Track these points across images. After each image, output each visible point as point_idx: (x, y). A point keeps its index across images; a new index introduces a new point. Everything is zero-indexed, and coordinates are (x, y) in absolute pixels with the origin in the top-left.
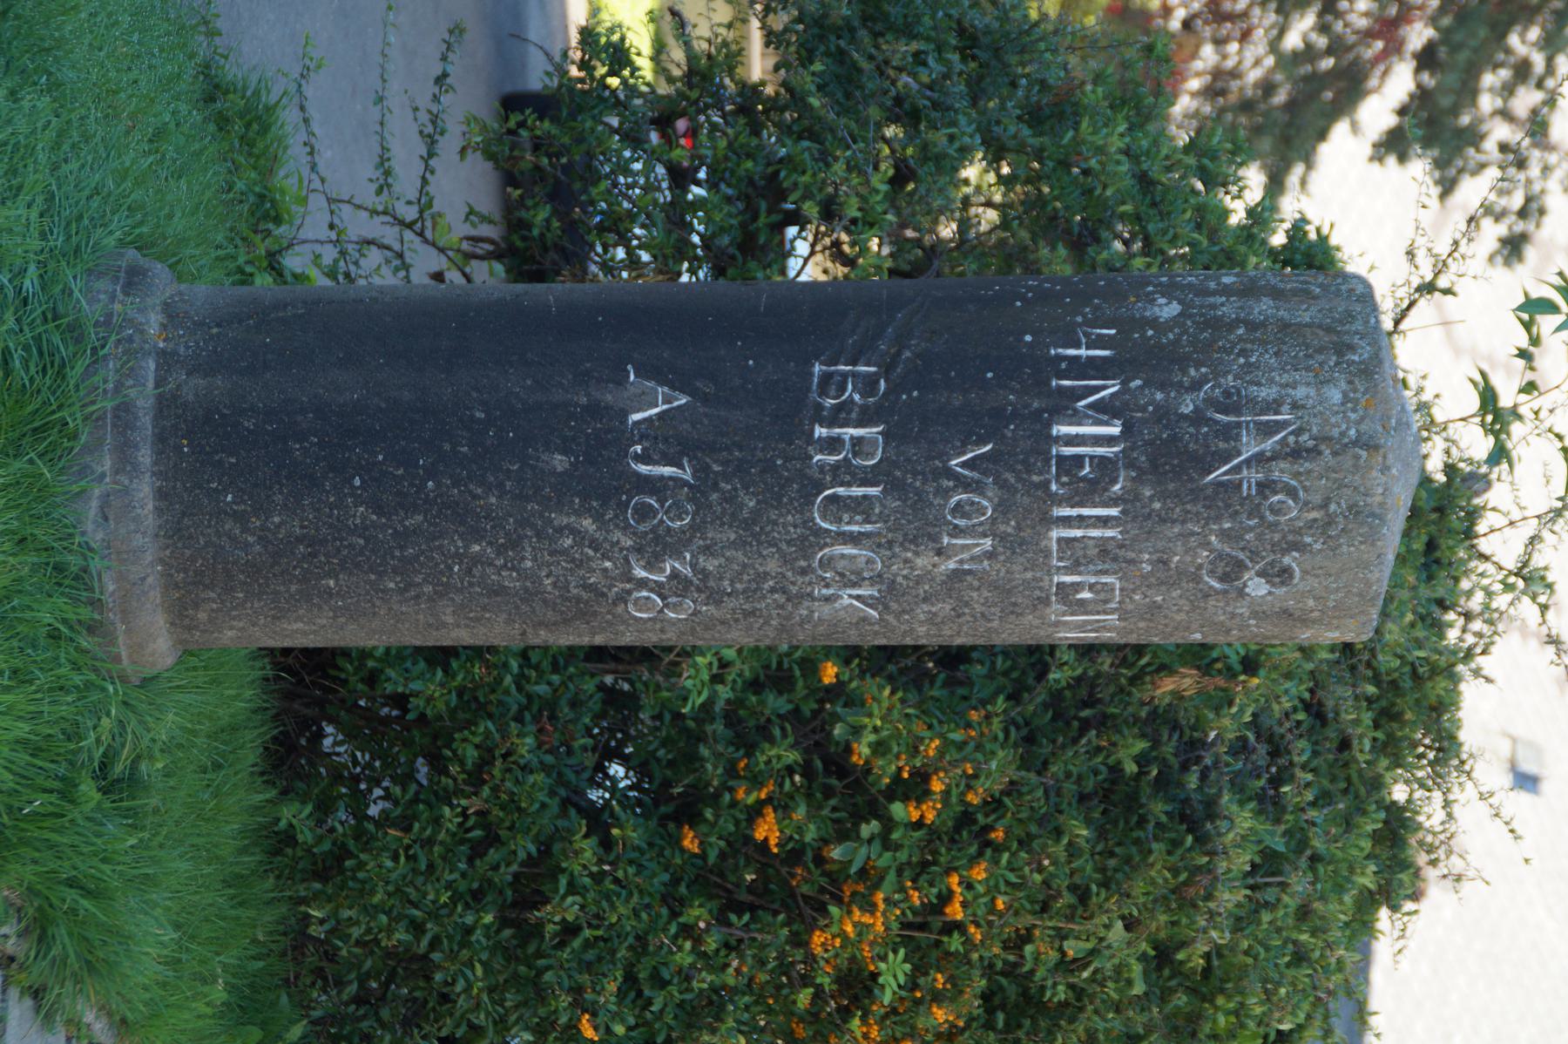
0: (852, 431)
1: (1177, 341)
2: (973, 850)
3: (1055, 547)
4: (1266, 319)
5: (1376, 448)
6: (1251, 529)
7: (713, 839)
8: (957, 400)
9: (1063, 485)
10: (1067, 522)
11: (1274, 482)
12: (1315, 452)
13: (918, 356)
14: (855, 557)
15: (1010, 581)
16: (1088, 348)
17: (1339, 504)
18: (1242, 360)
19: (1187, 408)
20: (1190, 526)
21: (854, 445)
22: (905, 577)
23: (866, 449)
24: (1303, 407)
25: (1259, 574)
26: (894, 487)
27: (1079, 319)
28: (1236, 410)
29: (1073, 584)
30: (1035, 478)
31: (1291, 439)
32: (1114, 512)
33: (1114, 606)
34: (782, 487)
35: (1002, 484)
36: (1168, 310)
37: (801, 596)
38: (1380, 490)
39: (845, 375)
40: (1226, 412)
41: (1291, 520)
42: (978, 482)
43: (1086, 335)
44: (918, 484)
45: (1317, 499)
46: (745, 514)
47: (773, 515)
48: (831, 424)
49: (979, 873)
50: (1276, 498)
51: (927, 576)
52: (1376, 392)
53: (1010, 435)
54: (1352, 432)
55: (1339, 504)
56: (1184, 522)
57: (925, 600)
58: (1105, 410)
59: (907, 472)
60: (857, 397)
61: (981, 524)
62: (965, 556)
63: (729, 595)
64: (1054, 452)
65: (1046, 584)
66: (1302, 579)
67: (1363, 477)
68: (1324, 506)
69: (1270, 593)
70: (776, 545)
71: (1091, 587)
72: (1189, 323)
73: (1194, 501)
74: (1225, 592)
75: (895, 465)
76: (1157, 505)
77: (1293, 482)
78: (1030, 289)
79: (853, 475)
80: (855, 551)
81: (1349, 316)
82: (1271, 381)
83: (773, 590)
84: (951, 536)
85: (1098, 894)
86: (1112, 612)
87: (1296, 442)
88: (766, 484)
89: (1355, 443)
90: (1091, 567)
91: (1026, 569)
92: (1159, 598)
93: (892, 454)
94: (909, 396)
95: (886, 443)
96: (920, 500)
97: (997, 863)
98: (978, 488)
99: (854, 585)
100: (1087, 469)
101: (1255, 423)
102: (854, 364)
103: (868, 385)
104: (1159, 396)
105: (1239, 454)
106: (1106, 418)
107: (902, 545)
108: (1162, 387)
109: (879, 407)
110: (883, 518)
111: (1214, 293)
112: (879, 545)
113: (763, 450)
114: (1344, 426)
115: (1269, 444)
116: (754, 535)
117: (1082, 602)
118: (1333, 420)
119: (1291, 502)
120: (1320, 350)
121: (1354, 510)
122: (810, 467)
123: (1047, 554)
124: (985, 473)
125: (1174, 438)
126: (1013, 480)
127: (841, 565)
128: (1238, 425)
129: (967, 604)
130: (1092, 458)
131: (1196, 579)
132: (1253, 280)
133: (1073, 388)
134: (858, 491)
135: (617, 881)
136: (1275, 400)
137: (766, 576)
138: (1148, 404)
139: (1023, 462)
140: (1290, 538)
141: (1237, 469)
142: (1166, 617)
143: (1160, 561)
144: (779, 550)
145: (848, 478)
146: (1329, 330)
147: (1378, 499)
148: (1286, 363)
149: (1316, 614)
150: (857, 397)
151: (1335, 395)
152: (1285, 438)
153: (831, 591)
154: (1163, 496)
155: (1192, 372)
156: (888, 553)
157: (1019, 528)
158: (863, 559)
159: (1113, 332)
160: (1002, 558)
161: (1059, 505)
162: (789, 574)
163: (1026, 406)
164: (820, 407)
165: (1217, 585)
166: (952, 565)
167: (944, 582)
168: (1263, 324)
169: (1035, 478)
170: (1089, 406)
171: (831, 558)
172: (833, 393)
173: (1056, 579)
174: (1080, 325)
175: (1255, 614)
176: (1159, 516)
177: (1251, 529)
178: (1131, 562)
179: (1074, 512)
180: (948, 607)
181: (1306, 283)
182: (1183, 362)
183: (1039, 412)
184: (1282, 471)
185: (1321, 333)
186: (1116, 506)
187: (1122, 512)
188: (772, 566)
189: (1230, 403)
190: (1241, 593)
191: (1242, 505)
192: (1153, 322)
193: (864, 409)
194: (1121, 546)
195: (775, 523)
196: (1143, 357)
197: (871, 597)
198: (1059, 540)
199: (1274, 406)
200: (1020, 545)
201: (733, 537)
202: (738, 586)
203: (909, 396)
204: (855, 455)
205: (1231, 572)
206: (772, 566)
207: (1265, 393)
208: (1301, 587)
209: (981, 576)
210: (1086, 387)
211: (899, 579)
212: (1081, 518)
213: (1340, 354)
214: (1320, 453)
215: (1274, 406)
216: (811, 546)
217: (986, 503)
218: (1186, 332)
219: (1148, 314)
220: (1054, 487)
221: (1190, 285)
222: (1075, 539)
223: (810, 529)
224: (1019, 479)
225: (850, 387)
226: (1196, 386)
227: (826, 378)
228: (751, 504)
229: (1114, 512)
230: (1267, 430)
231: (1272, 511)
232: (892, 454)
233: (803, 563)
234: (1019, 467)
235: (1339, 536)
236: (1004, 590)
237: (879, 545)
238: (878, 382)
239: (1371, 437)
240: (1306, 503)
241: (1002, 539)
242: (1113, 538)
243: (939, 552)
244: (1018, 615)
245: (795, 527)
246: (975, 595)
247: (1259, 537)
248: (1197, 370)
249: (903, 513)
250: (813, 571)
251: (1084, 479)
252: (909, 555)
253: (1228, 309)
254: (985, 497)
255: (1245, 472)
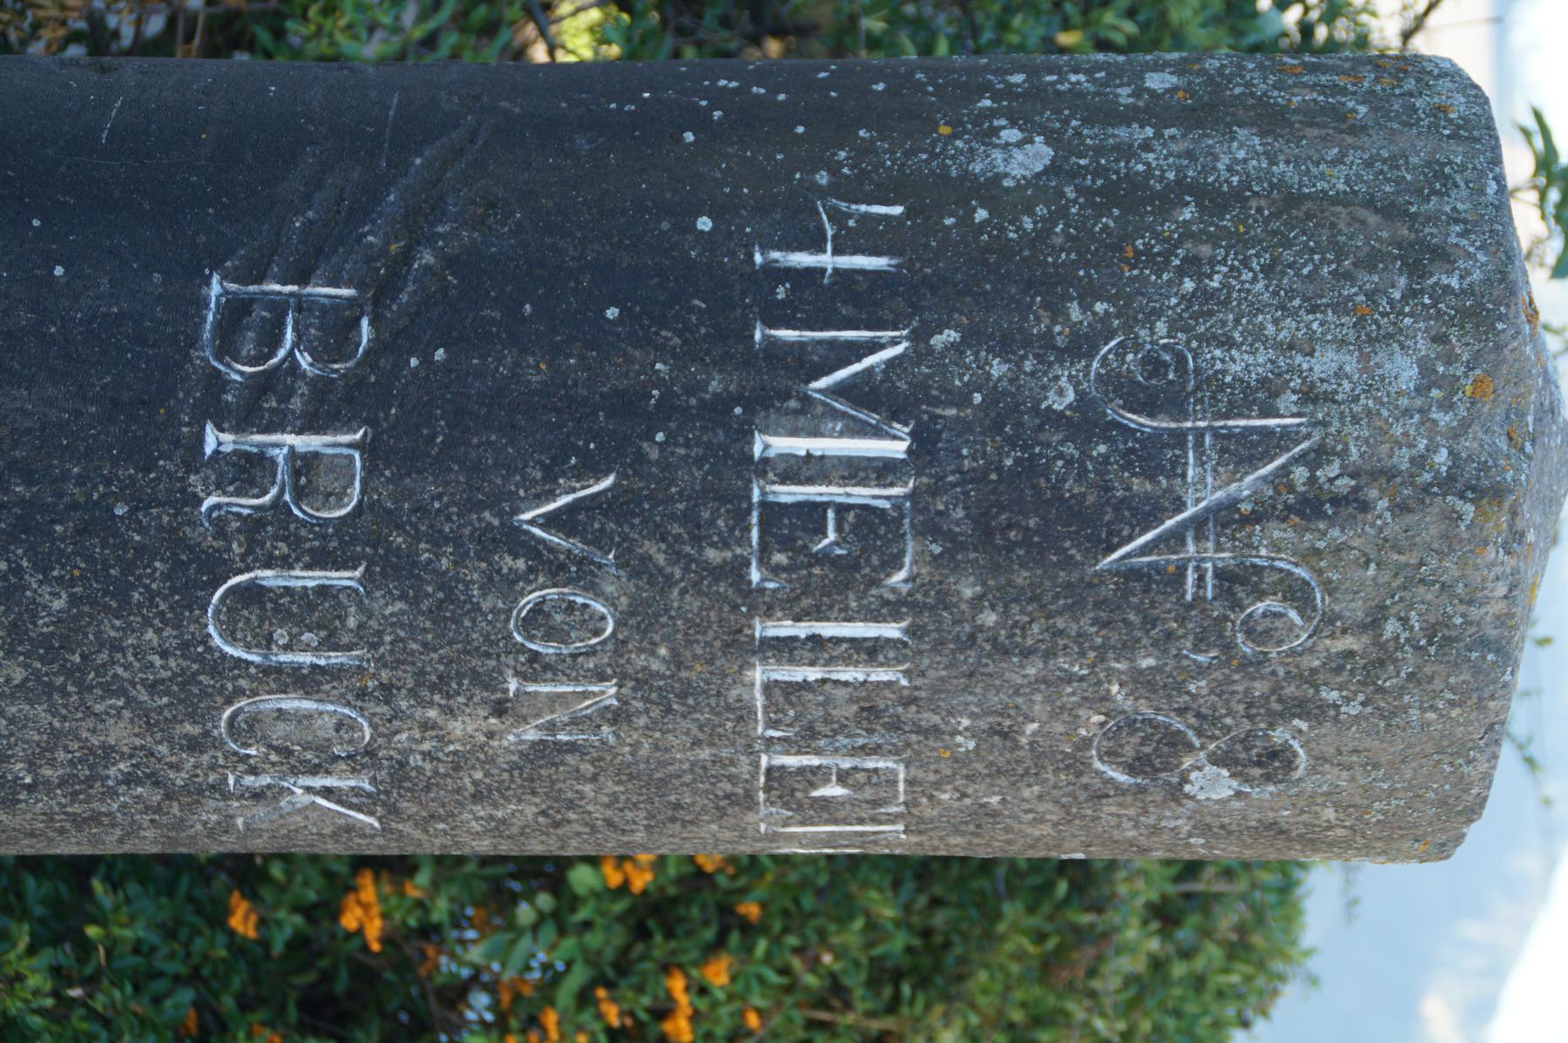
0: (290, 439)
1: (1042, 235)
2: (709, 934)
3: (760, 701)
4: (1246, 184)
5: (1497, 493)
6: (1202, 671)
7: (282, 914)
8: (537, 371)
9: (776, 570)
10: (784, 649)
11: (1257, 570)
12: (1355, 503)
13: (450, 262)
14: (309, 716)
15: (662, 764)
16: (837, 251)
17: (1404, 621)
18: (1189, 285)
19: (1062, 399)
20: (1063, 662)
21: (296, 473)
22: (426, 755)
23: (324, 482)
24: (1330, 398)
25: (1215, 760)
26: (393, 570)
27: (823, 178)
28: (1174, 403)
29: (801, 770)
30: (712, 555)
31: (1300, 474)
32: (892, 631)
33: (893, 809)
34: (129, 567)
35: (638, 568)
36: (1023, 158)
37: (196, 792)
38: (1502, 590)
39: (278, 307)
40: (1149, 407)
41: (1293, 652)
42: (580, 562)
43: (837, 217)
44: (445, 563)
45: (1356, 609)
46: (44, 625)
47: (111, 628)
48: (245, 420)
49: (718, 974)
50: (1260, 607)
51: (477, 754)
52: (1497, 365)
53: (654, 454)
54: (1442, 457)
55: (1404, 621)
56: (1049, 655)
57: (477, 797)
58: (873, 400)
59: (418, 538)
60: (304, 360)
61: (591, 652)
62: (561, 716)
63: (30, 788)
64: (756, 496)
65: (744, 767)
66: (1312, 770)
67: (1463, 563)
68: (1373, 624)
69: (1238, 794)
70: (122, 692)
71: (843, 777)
72: (1070, 192)
73: (1075, 609)
74: (1141, 790)
75: (392, 519)
76: (990, 618)
77: (1300, 572)
78: (719, 98)
79: (296, 542)
80: (308, 705)
81: (1438, 178)
82: (1257, 335)
83: (129, 780)
84: (522, 676)
85: (912, 1002)
86: (893, 819)
87: (1312, 480)
88: (90, 559)
89: (1448, 483)
90: (842, 740)
91: (697, 743)
92: (995, 800)
93: (384, 495)
94: (427, 360)
95: (370, 471)
96: (450, 598)
97: (749, 949)
98: (583, 574)
99: (314, 770)
100: (832, 536)
101: (1216, 434)
102: (303, 280)
103: (333, 330)
104: (998, 369)
105: (1180, 506)
106: (873, 419)
107: (413, 693)
108: (1005, 346)
109: (355, 383)
110: (367, 637)
111: (1129, 117)
112: (362, 694)
113: (81, 481)
114: (1422, 444)
115: (1247, 485)
116: (68, 671)
117: (826, 802)
118: (1398, 430)
119: (1293, 615)
120: (1370, 262)
121: (1439, 635)
122: (194, 524)
123: (744, 713)
124: (599, 541)
125: (1031, 468)
126: (661, 559)
127: (279, 732)
128: (1179, 438)
129: (571, 805)
130: (842, 509)
131: (1077, 765)
132: (1216, 82)
133: (801, 345)
134: (306, 579)
135: (93, 1015)
136: (1263, 382)
137: (108, 753)
138: (971, 388)
139: (688, 518)
140: (1290, 690)
141: (1174, 539)
142: (1008, 830)
143: (994, 731)
144: (130, 701)
145: (283, 548)
146: (1391, 211)
147: (1498, 607)
148: (1291, 293)
149: (1340, 832)
150: (304, 360)
151: (1404, 371)
152: (1285, 470)
153: (265, 780)
154: (1003, 599)
155: (1075, 312)
156: (384, 709)
157: (677, 661)
158: (330, 722)
159: (897, 210)
160: (642, 721)
161: (768, 613)
162: (163, 749)
163: (694, 388)
164: (216, 382)
165: (1122, 778)
166: (531, 735)
167: (514, 767)
168: (1239, 196)
169: (712, 555)
170: (839, 391)
171: (254, 721)
172: (248, 348)
173: (764, 760)
174: (823, 193)
175: (1204, 829)
176: (994, 640)
177: (1202, 671)
178: (935, 731)
179: (802, 630)
180: (530, 811)
181: (1335, 89)
182: (1052, 288)
183: (722, 405)
184: (1276, 547)
185: (1373, 220)
186: (896, 617)
187: (911, 631)
188: (120, 733)
189: (1161, 388)
190: (1176, 794)
191: (1182, 620)
192: (989, 189)
193: (321, 388)
194: (908, 702)
195: (117, 647)
196: (967, 275)
197: (357, 792)
198: (768, 687)
199: (1262, 395)
200: (682, 696)
201: (19, 675)
202: (47, 772)
203: (427, 360)
204: (300, 494)
205: (1156, 757)
206: (120, 733)
207: (1242, 364)
208: (1308, 786)
209: (601, 757)
210: (832, 343)
211: (415, 760)
212: (815, 639)
213: (1416, 270)
214: (1365, 507)
215: (1262, 395)
216: (204, 694)
217: (599, 608)
218: (1062, 213)
219: (977, 167)
220: (755, 575)
221: (1076, 93)
222: (805, 685)
223: (200, 658)
224: (676, 556)
225: (289, 335)
226: (1082, 345)
227: (236, 311)
228: (58, 604)
229: (892, 631)
230: (1243, 451)
231: (1250, 633)
232: (384, 495)
233: (189, 728)
234: (677, 529)
235: (1401, 690)
236: (652, 783)
237: (362, 694)
238: (355, 324)
239: (1484, 467)
240: (1330, 619)
241: (639, 684)
242: (889, 685)
243: (500, 710)
244: (684, 824)
245: (164, 654)
246: (587, 789)
247: (1219, 689)
248: (1086, 307)
249: (412, 628)
250: (218, 744)
251: (824, 558)
252: (432, 713)
253: (1160, 156)
254: (598, 594)
255: (1191, 548)
